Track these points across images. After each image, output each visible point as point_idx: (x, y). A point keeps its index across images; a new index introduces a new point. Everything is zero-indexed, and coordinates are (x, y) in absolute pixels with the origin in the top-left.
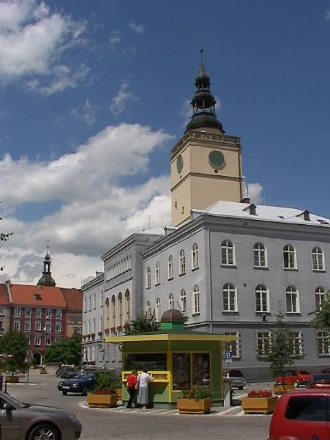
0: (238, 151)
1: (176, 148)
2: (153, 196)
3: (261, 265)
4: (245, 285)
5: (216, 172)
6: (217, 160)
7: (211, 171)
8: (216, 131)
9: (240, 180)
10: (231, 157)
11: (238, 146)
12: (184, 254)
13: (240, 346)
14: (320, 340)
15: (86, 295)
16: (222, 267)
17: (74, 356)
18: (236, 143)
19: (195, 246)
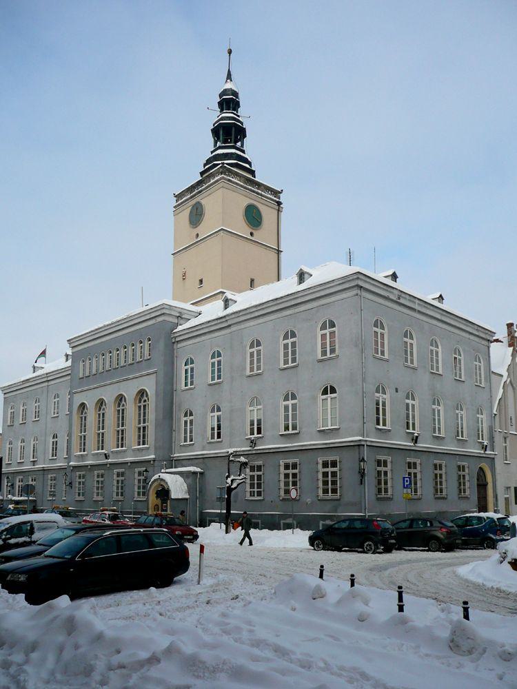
5: (252, 234)
14: (379, 473)
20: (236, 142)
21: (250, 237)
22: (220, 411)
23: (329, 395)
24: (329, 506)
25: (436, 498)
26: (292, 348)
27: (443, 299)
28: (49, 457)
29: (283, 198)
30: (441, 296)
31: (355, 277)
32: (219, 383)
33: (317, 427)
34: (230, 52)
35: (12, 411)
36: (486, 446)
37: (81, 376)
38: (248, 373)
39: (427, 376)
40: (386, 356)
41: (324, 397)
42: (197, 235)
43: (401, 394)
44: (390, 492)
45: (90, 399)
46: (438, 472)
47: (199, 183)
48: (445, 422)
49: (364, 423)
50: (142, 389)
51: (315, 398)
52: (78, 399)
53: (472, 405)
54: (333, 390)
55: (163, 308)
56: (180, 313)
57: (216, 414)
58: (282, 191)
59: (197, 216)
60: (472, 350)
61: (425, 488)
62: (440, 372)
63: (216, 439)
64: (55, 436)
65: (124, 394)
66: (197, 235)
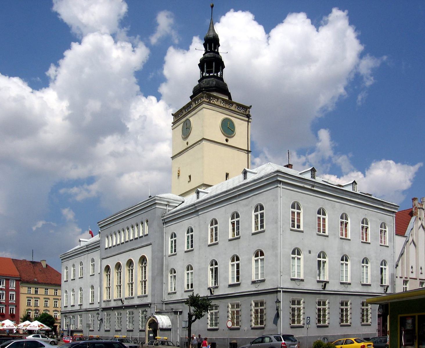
0: (248, 122)
1: (181, 111)
2: (268, 42)
3: (323, 232)
4: (310, 252)
5: (227, 140)
6: (228, 129)
7: (222, 138)
8: (227, 98)
9: (248, 152)
10: (240, 125)
11: (248, 116)
12: (82, 265)
13: (228, 312)
14: (293, 310)
15: (289, 163)
16: (291, 230)
17: (92, 344)
18: (244, 111)
19: (93, 260)
20: (217, 72)
21: (225, 142)
22: (217, 265)
23: (259, 257)
24: (259, 332)
25: (318, 327)
26: (215, 231)
27: (356, 184)
28: (227, 279)
29: (252, 112)
30: (354, 182)
31: (276, 174)
32: (192, 250)
33: (78, 303)
34: (212, 7)
35: (67, 271)
36: (388, 286)
37: (107, 247)
38: (209, 243)
39: (338, 240)
40: (302, 229)
41: (257, 258)
42: (187, 143)
43: (314, 255)
44: (327, 322)
45: (111, 263)
46: (322, 307)
47: (189, 105)
48: (351, 273)
49: (281, 276)
50: (143, 256)
51: (250, 260)
52: (106, 262)
53: (377, 260)
54: (262, 254)
55: (155, 199)
56: (168, 202)
57: (235, 262)
58: (251, 106)
59: (187, 131)
60: (378, 220)
61: (332, 317)
62: (349, 238)
63: (190, 289)
64: (92, 287)
65: (132, 259)
66: (187, 143)
